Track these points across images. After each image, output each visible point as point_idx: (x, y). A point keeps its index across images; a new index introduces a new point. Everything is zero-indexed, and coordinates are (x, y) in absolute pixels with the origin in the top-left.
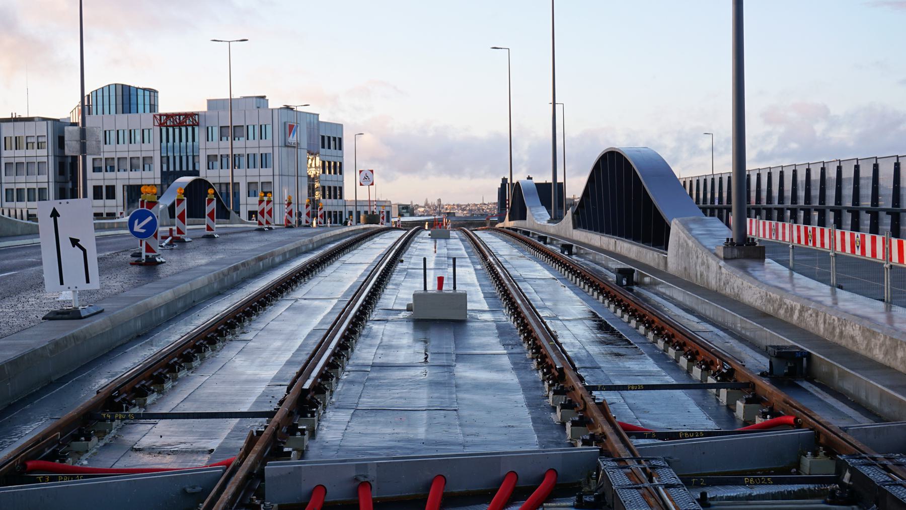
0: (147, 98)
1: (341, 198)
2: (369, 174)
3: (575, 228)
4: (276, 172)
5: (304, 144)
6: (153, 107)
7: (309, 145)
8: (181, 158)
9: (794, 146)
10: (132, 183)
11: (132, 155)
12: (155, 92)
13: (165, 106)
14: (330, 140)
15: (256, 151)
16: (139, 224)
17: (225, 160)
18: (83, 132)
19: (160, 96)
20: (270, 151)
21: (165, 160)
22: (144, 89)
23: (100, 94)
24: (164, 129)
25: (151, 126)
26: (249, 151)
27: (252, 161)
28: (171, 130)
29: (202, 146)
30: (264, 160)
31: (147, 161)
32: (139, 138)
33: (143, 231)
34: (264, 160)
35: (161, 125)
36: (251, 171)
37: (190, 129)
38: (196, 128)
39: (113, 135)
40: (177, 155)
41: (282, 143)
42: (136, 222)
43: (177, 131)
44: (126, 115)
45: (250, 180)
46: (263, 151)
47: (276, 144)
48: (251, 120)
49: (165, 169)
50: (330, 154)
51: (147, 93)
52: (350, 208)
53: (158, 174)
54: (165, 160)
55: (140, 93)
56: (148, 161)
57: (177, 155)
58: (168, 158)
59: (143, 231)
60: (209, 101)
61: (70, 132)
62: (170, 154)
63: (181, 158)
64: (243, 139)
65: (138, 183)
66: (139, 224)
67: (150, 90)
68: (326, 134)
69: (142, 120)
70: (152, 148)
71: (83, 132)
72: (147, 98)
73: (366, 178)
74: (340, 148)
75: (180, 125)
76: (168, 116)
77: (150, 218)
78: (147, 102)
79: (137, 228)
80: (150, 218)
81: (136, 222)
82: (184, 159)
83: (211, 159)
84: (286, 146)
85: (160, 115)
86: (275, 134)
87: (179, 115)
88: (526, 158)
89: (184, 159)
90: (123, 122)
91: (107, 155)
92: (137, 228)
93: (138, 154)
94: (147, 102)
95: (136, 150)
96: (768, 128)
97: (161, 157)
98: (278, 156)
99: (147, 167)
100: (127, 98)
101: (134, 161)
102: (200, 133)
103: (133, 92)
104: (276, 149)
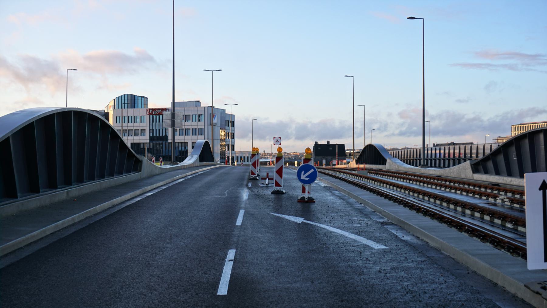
0: (143, 101)
1: (233, 150)
2: (279, 139)
3: (474, 172)
5: (219, 124)
6: (146, 104)
7: (221, 124)
8: (159, 130)
9: (415, 128)
10: (135, 142)
11: (135, 128)
12: (147, 98)
13: (151, 105)
14: (228, 122)
15: (196, 127)
16: (304, 174)
17: (181, 131)
18: (173, 115)
19: (148, 99)
20: (203, 127)
21: (151, 131)
22: (141, 97)
23: (123, 99)
24: (151, 116)
25: (145, 114)
26: (193, 127)
28: (155, 116)
30: (201, 132)
31: (143, 131)
32: (139, 120)
33: (307, 179)
34: (201, 132)
35: (150, 114)
36: (194, 137)
39: (126, 119)
40: (157, 128)
41: (209, 123)
42: (303, 173)
43: (158, 117)
44: (133, 109)
45: (193, 141)
46: (200, 127)
47: (206, 124)
48: (194, 112)
49: (151, 135)
50: (228, 129)
51: (143, 99)
52: (237, 155)
53: (148, 138)
54: (151, 131)
55: (140, 98)
56: (143, 131)
57: (157, 128)
58: (153, 130)
59: (307, 179)
61: (167, 115)
62: (154, 128)
63: (159, 130)
64: (190, 122)
65: (138, 142)
66: (304, 174)
67: (144, 97)
68: (227, 119)
69: (139, 112)
70: (146, 125)
71: (173, 115)
72: (143, 101)
73: (277, 141)
74: (233, 126)
75: (159, 114)
76: (153, 110)
77: (312, 170)
78: (143, 103)
79: (303, 177)
80: (312, 170)
81: (303, 173)
82: (161, 130)
85: (150, 109)
86: (206, 119)
87: (159, 109)
88: (294, 132)
89: (161, 130)
90: (131, 112)
91: (187, 127)
92: (303, 177)
93: (138, 128)
94: (143, 103)
95: (138, 126)
96: (402, 121)
97: (150, 130)
98: (208, 130)
99: (142, 134)
100: (132, 101)
101: (136, 131)
103: (136, 98)
104: (206, 126)
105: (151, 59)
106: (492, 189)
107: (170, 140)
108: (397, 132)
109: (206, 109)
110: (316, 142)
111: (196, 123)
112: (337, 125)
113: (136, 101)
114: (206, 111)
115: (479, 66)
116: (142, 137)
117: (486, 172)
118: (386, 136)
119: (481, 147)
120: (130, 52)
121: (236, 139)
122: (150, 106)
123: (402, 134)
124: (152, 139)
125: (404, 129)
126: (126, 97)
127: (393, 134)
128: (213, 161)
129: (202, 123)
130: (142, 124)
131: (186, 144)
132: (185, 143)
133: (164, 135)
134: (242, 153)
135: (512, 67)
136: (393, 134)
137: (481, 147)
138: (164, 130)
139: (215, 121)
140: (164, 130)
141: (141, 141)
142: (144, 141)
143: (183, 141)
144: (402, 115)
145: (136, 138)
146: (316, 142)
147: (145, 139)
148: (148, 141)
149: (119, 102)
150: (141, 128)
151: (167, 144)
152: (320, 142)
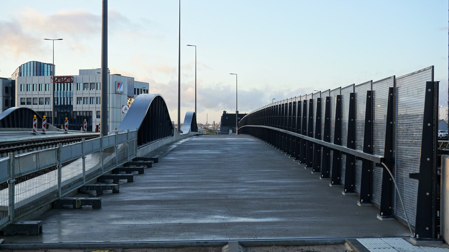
5: (126, 92)
6: (52, 73)
8: (64, 98)
11: (40, 96)
17: (85, 100)
22: (48, 64)
23: (26, 66)
24: (56, 84)
28: (59, 84)
29: (74, 93)
37: (69, 84)
38: (72, 84)
43: (62, 85)
44: (37, 77)
51: (49, 66)
55: (46, 66)
56: (48, 100)
57: (62, 96)
58: (58, 98)
60: (80, 70)
63: (64, 98)
65: (43, 110)
68: (137, 87)
69: (47, 79)
70: (49, 93)
75: (64, 82)
83: (79, 99)
84: (116, 93)
87: (64, 77)
90: (36, 80)
93: (43, 96)
99: (47, 102)
100: (39, 68)
101: (41, 100)
102: (74, 86)
103: (42, 65)
106: (27, 144)
107: (447, 133)
110: (225, 112)
113: (42, 68)
124: (55, 106)
126: (32, 63)
131: (91, 112)
132: (90, 112)
133: (69, 104)
139: (120, 90)
141: (46, 110)
142: (49, 110)
143: (87, 110)
146: (225, 112)
147: (49, 108)
148: (52, 110)
151: (72, 112)
152: (229, 112)
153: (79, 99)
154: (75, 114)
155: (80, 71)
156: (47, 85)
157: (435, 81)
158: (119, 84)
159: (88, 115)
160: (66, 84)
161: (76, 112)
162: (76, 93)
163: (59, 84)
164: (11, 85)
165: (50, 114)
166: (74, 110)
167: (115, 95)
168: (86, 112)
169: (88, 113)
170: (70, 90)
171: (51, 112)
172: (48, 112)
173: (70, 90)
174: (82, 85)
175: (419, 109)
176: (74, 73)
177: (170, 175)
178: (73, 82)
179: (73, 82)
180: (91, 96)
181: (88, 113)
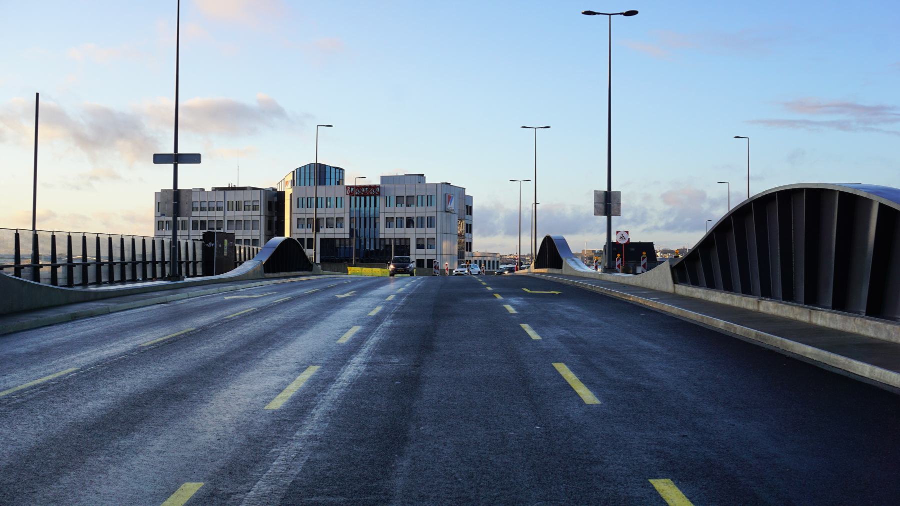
2: (625, 234)
4: (439, 231)
5: (456, 211)
6: (340, 181)
10: (327, 236)
15: (423, 215)
20: (434, 215)
22: (336, 168)
23: (303, 170)
24: (353, 198)
27: (421, 222)
37: (373, 198)
38: (378, 198)
43: (363, 199)
45: (418, 236)
46: (429, 215)
47: (439, 210)
55: (333, 170)
56: (300, 221)
65: (332, 236)
70: (343, 212)
75: (365, 195)
83: (389, 221)
87: (365, 187)
93: (332, 216)
96: (667, 208)
99: (339, 225)
100: (321, 174)
102: (381, 201)
103: (328, 170)
104: (439, 214)
105: (278, 112)
108: (661, 224)
109: (439, 187)
111: (423, 209)
112: (569, 212)
114: (439, 190)
115: (792, 123)
116: (339, 230)
117: (695, 283)
118: (644, 230)
119: (116, 243)
120: (250, 98)
121: (474, 231)
122: (349, 181)
123: (669, 227)
125: (671, 220)
127: (656, 228)
128: (561, 267)
129: (433, 208)
130: (339, 210)
134: (484, 255)
135: (842, 126)
136: (656, 228)
137: (116, 243)
138: (372, 220)
139: (451, 206)
140: (372, 220)
141: (337, 236)
142: (342, 236)
143: (402, 236)
144: (666, 198)
145: (399, 230)
148: (347, 236)
149: (301, 175)
150: (337, 216)
153: (389, 221)
154: (382, 242)
155: (383, 178)
156: (339, 200)
157: (172, 166)
158: (450, 197)
159: (403, 243)
160: (368, 198)
161: (385, 239)
162: (385, 210)
163: (358, 198)
164: (276, 199)
165: (343, 243)
166: (382, 236)
167: (445, 214)
168: (400, 239)
169: (403, 241)
170: (375, 206)
171: (345, 239)
172: (340, 239)
173: (375, 206)
174: (393, 200)
175: (30, 252)
176: (374, 180)
177: (46, 375)
178: (379, 195)
179: (379, 195)
180: (203, 219)
181: (403, 241)
